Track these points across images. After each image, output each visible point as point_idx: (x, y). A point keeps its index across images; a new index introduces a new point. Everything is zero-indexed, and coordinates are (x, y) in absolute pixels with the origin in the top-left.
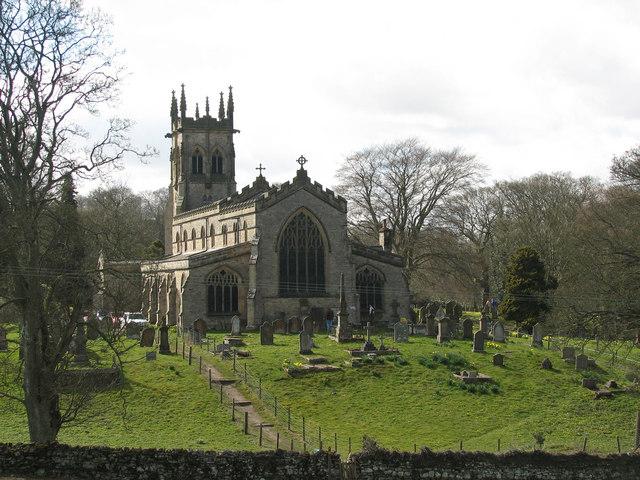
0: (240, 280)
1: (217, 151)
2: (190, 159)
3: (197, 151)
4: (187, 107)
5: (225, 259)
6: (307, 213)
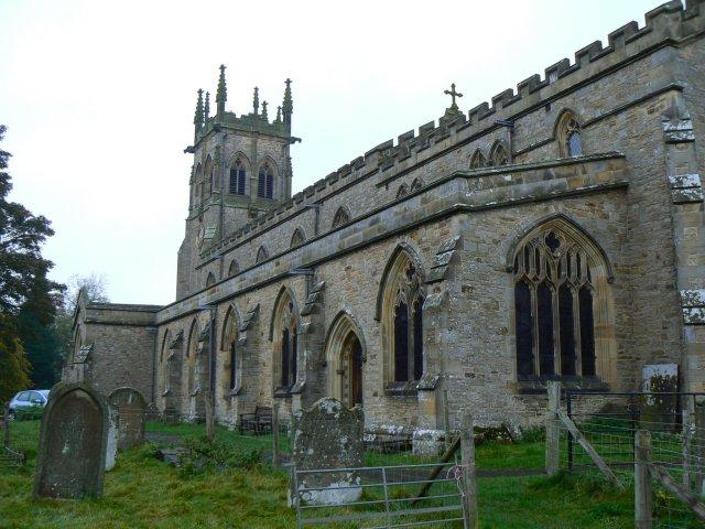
2: (228, 171)
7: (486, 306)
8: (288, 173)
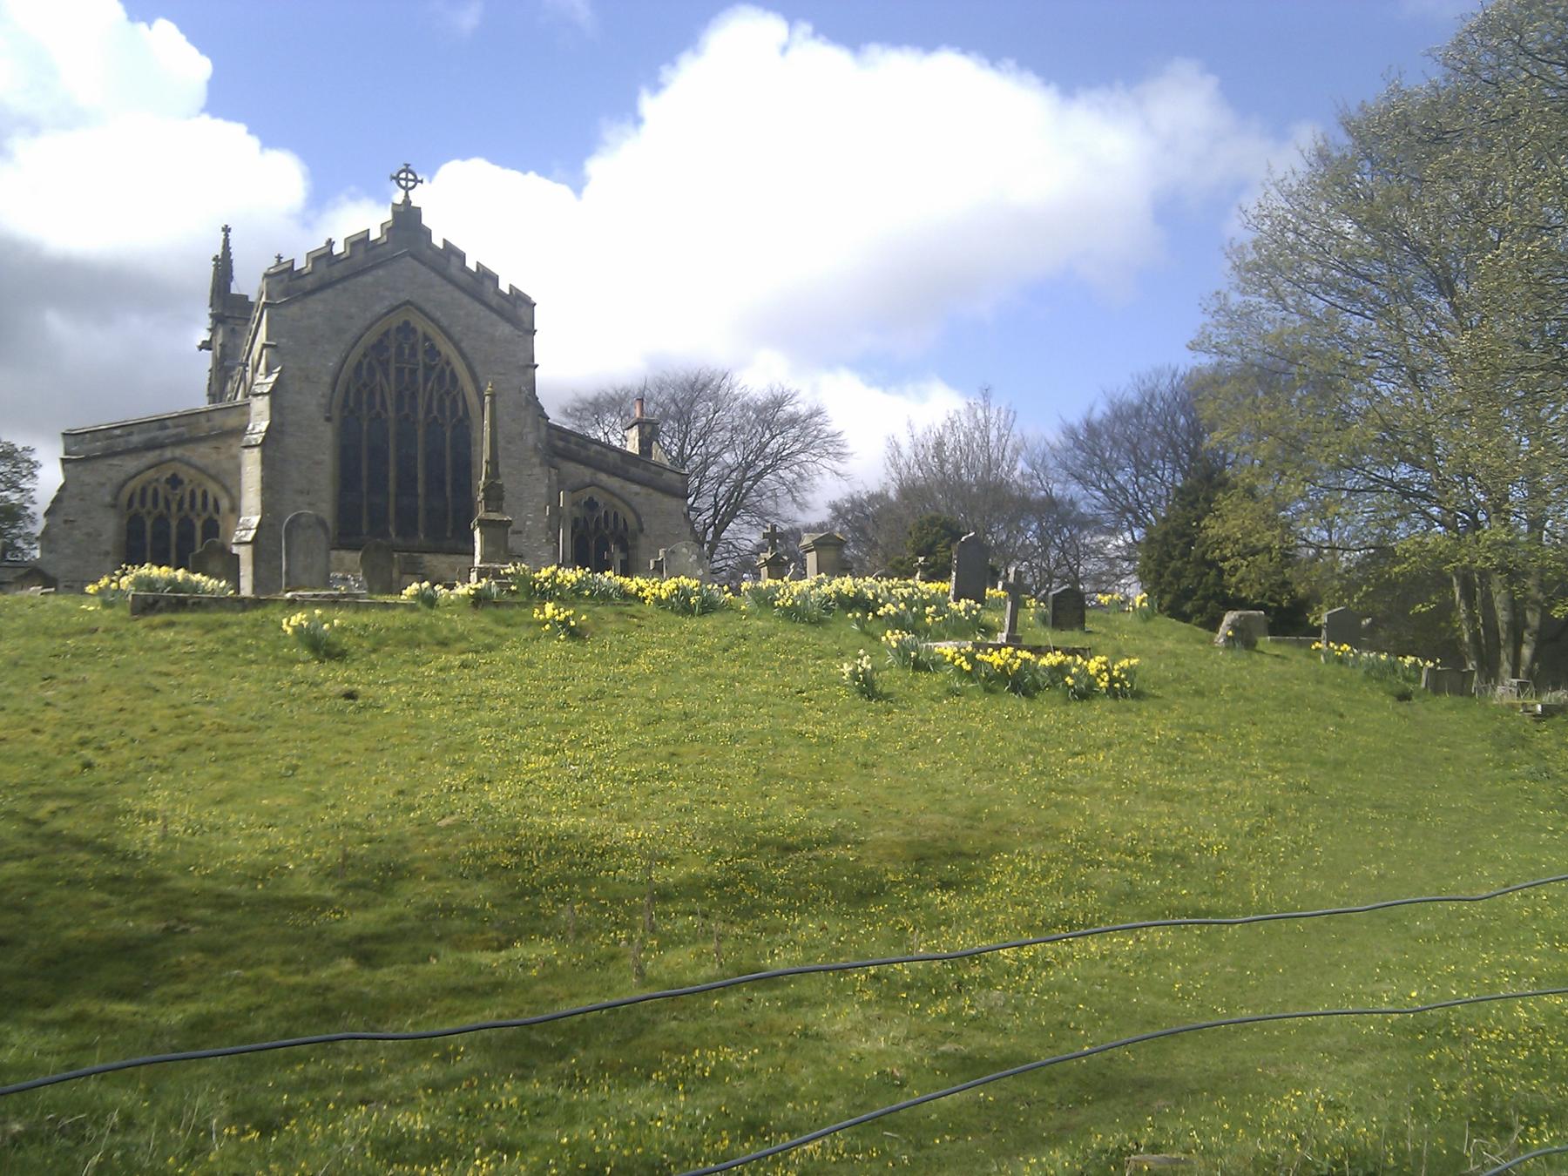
5: (179, 441)
6: (421, 325)
7: (89, 535)
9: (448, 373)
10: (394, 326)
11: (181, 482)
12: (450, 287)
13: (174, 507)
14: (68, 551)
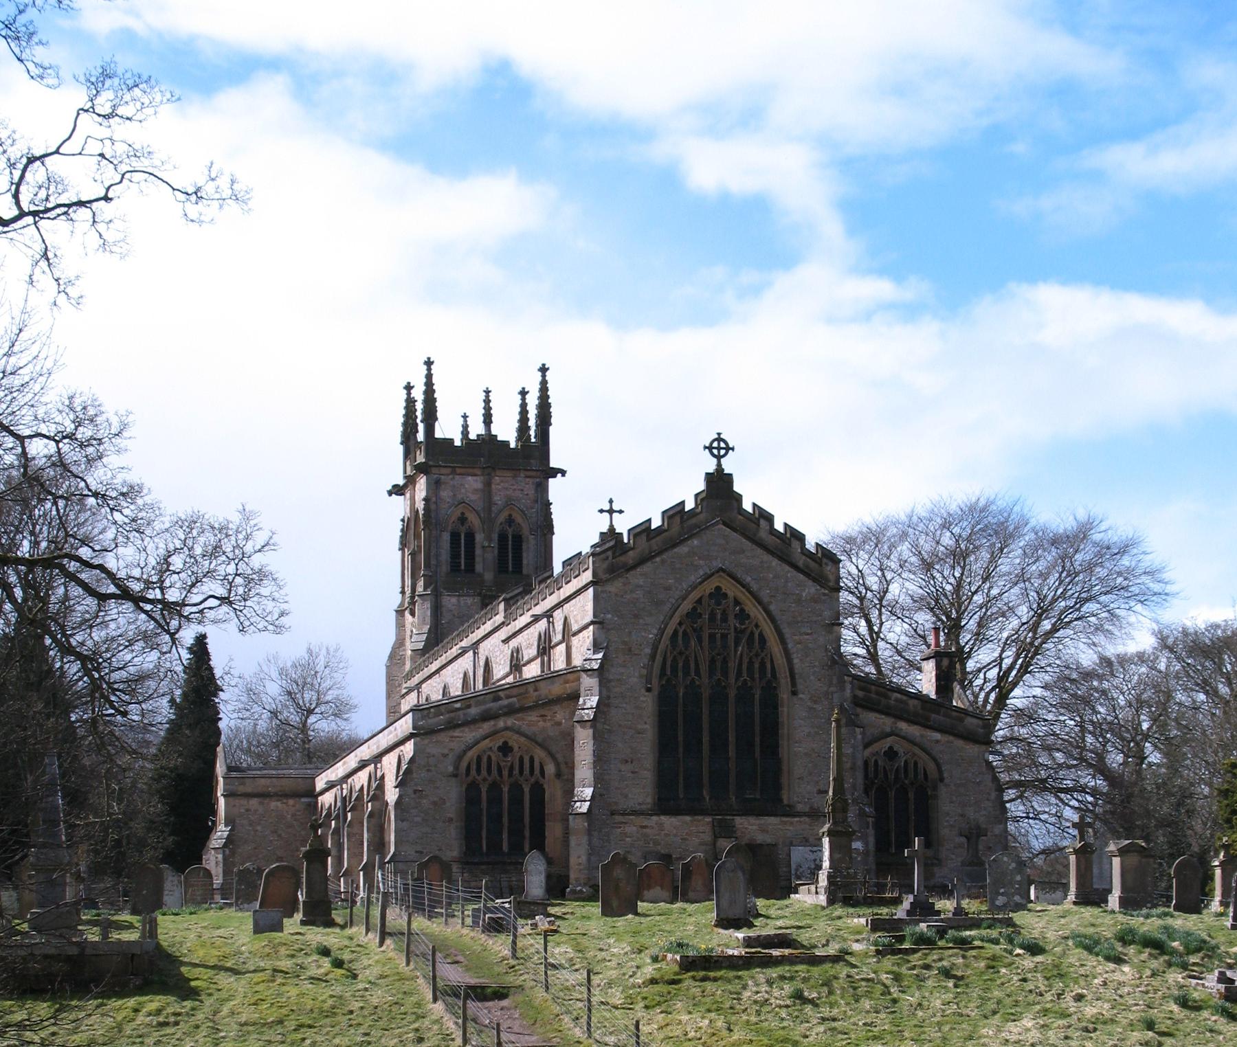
0: (550, 769)
1: (510, 521)
2: (446, 537)
3: (463, 519)
4: (440, 414)
5: (511, 711)
6: (731, 589)
7: (435, 803)
8: (546, 528)
9: (756, 636)
10: (708, 592)
11: (511, 749)
12: (759, 551)
13: (505, 773)
14: (418, 819)
